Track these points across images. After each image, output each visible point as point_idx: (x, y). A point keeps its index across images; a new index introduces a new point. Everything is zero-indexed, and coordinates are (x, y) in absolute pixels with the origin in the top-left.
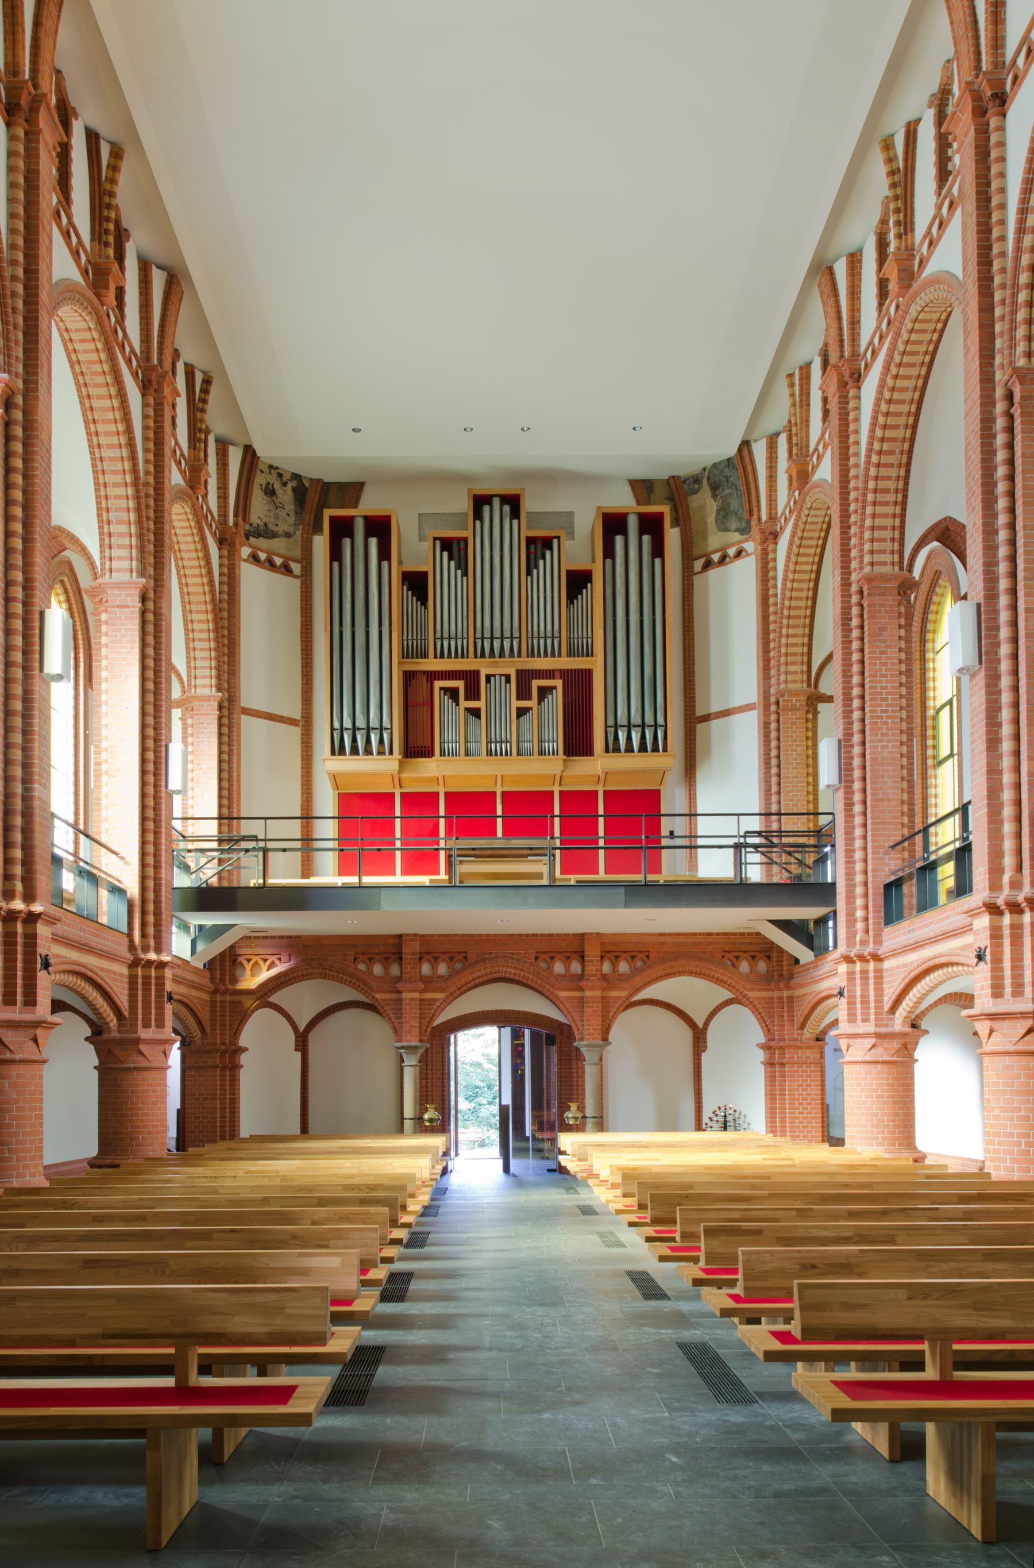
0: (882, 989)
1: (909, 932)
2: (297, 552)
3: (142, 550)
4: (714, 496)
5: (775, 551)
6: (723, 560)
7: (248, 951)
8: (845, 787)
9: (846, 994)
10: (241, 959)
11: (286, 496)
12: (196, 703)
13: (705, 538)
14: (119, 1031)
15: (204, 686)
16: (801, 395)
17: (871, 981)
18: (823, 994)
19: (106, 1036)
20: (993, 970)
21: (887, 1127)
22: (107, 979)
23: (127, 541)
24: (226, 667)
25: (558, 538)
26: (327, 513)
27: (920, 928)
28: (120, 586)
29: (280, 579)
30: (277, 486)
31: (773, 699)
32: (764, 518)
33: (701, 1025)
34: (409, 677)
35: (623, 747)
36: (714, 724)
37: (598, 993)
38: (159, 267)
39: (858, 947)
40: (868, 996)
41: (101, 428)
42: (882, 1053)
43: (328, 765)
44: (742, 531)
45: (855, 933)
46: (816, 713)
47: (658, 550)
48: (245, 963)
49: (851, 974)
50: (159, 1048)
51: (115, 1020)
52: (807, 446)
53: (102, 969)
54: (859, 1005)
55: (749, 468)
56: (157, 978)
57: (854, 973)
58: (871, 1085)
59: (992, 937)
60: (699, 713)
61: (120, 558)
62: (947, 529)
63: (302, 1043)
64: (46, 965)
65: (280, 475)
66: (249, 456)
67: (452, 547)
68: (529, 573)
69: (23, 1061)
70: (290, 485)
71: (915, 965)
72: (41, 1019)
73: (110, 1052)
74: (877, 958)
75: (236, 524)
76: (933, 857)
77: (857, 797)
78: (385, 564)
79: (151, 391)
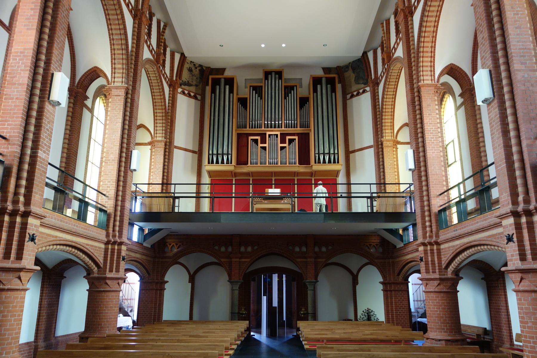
0: (441, 258)
1: (454, 231)
2: (200, 92)
3: (128, 75)
4: (354, 72)
5: (378, 89)
6: (358, 94)
7: (169, 241)
8: (418, 170)
9: (424, 260)
10: (167, 244)
11: (196, 72)
12: (156, 143)
13: (351, 87)
14: (98, 274)
15: (159, 137)
16: (386, 30)
17: (436, 254)
18: (409, 261)
19: (91, 276)
20: (519, 246)
21: (448, 323)
22: (90, 249)
23: (121, 71)
24: (169, 130)
25: (296, 86)
26: (211, 77)
27: (460, 229)
28: (117, 88)
29: (193, 101)
30: (193, 68)
31: (380, 143)
32: (373, 78)
33: (355, 273)
34: (239, 136)
35: (322, 162)
36: (357, 153)
37: (313, 260)
38: (351, 320)
39: (428, 239)
40: (434, 261)
41: (113, 27)
42: (442, 288)
43: (207, 167)
44: (365, 84)
45: (426, 233)
46: (397, 148)
47: (334, 90)
48: (169, 245)
49: (425, 251)
50: (116, 282)
51: (96, 268)
52: (390, 47)
53: (88, 245)
54: (430, 265)
55: (367, 61)
56: (118, 250)
57: (427, 250)
58: (439, 303)
59: (516, 228)
60: (351, 149)
61: (118, 77)
62: (452, 68)
63: (192, 279)
64: (32, 239)
65: (194, 65)
66: (183, 57)
67: (258, 90)
68: (285, 98)
69: (9, 290)
70: (198, 68)
71: (459, 246)
72: (24, 267)
73: (93, 283)
74: (438, 244)
75: (176, 80)
76: (487, 184)
77: (423, 173)
78: (231, 95)
79: (138, 18)
